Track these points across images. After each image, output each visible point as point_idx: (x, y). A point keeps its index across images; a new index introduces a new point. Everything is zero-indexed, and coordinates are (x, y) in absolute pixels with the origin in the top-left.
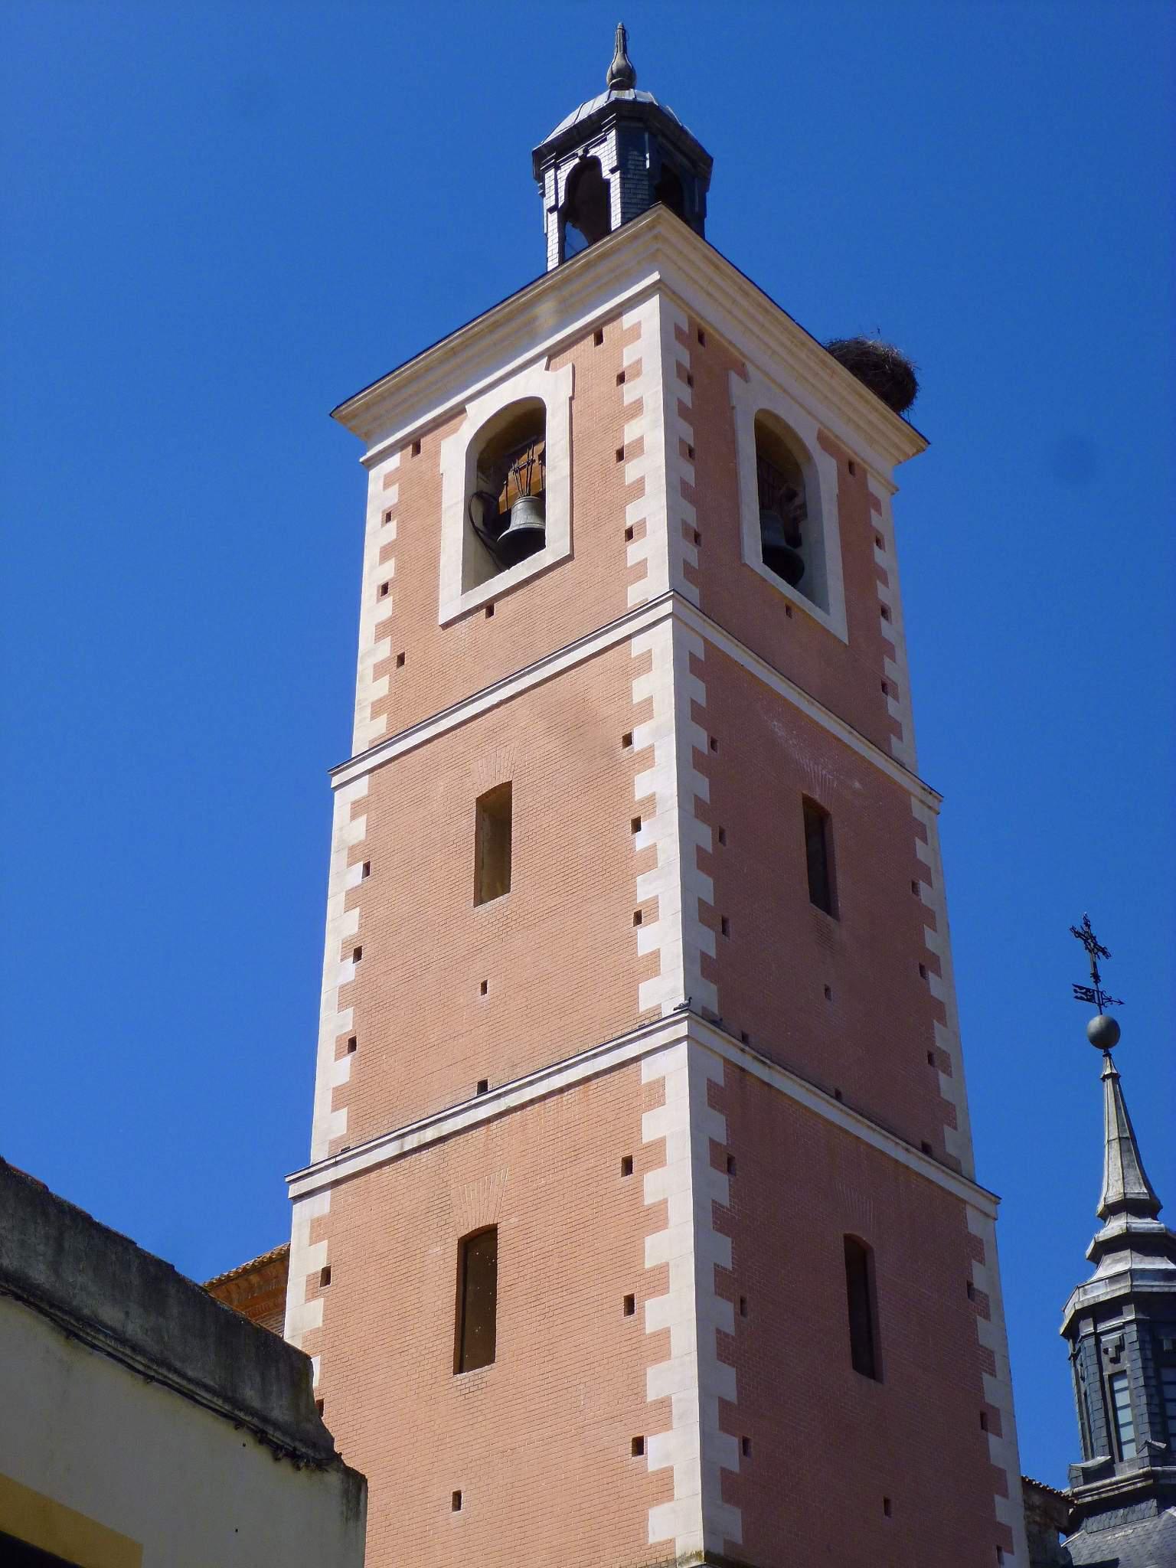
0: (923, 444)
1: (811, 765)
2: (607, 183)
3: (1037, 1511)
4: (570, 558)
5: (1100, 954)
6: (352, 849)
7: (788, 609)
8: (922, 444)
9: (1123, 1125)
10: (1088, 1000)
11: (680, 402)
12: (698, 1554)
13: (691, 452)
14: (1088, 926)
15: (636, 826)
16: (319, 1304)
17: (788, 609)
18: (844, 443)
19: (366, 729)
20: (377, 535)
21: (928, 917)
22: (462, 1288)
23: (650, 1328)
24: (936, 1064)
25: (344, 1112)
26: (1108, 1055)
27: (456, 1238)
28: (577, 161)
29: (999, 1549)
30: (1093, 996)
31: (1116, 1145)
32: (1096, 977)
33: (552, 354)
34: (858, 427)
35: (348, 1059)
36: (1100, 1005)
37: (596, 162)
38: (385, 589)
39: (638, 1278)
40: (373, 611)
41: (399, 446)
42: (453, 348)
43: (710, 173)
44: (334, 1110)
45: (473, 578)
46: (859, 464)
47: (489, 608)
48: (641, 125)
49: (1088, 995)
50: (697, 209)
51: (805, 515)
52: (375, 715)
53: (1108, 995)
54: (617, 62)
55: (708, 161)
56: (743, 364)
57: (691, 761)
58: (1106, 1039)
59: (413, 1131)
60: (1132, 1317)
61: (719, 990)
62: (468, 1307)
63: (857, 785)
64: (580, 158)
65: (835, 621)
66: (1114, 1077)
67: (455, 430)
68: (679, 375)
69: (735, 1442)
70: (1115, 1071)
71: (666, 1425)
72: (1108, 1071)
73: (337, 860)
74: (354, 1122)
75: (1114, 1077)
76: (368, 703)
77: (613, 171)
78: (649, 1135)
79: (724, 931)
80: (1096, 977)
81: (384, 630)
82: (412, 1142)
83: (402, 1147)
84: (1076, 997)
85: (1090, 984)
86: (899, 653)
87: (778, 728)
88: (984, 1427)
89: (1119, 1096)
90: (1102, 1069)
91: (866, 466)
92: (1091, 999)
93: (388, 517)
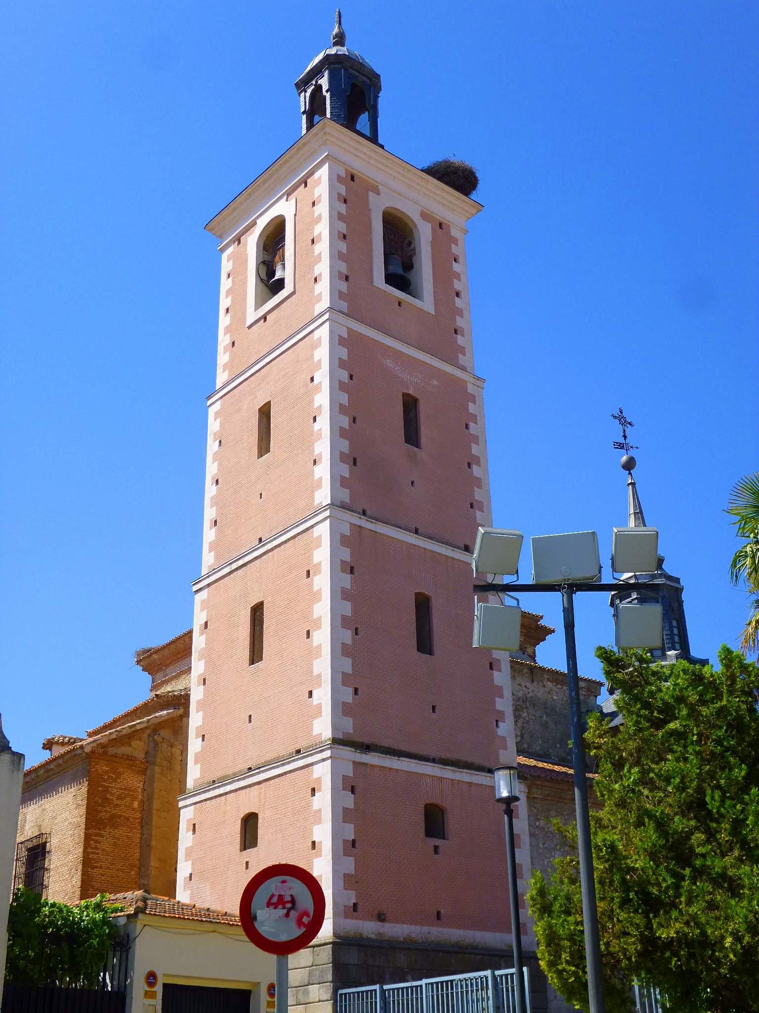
0: (480, 208)
1: (408, 378)
2: (325, 97)
3: (584, 689)
4: (293, 293)
5: (628, 425)
6: (215, 434)
7: (400, 304)
8: (479, 208)
9: (636, 506)
10: (620, 448)
11: (339, 213)
12: (330, 739)
13: (345, 237)
14: (621, 413)
15: (315, 419)
16: (204, 637)
17: (400, 304)
18: (436, 214)
19: (222, 377)
20: (225, 284)
21: (476, 439)
22: (253, 630)
23: (315, 644)
24: (474, 508)
25: (213, 553)
26: (630, 474)
27: (250, 607)
28: (313, 87)
29: (497, 721)
30: (623, 446)
31: (632, 516)
32: (625, 437)
33: (289, 194)
34: (444, 205)
35: (214, 530)
36: (626, 450)
37: (320, 87)
38: (227, 310)
39: (311, 623)
40: (224, 321)
41: (232, 242)
42: (249, 194)
43: (380, 82)
44: (209, 553)
45: (260, 303)
46: (445, 223)
47: (264, 318)
48: (340, 66)
49: (621, 446)
50: (372, 103)
51: (415, 253)
52: (224, 370)
53: (631, 445)
54: (336, 30)
55: (378, 77)
56: (377, 186)
57: (338, 386)
58: (629, 466)
59: (235, 561)
60: (636, 597)
61: (350, 492)
62: (256, 637)
63: (435, 382)
64: (315, 85)
65: (427, 303)
66: (633, 484)
67: (252, 233)
68: (339, 200)
69: (351, 690)
70: (633, 481)
71: (320, 685)
72: (630, 482)
73: (210, 439)
74: (217, 557)
75: (633, 484)
76: (221, 365)
77: (327, 91)
78: (315, 561)
79: (355, 464)
80: (625, 437)
81: (228, 330)
82: (234, 566)
83: (231, 568)
84: (615, 448)
85: (622, 441)
86: (465, 313)
87: (389, 363)
88: (491, 668)
89: (635, 493)
90: (627, 480)
91: (449, 223)
92: (622, 448)
93: (229, 276)
